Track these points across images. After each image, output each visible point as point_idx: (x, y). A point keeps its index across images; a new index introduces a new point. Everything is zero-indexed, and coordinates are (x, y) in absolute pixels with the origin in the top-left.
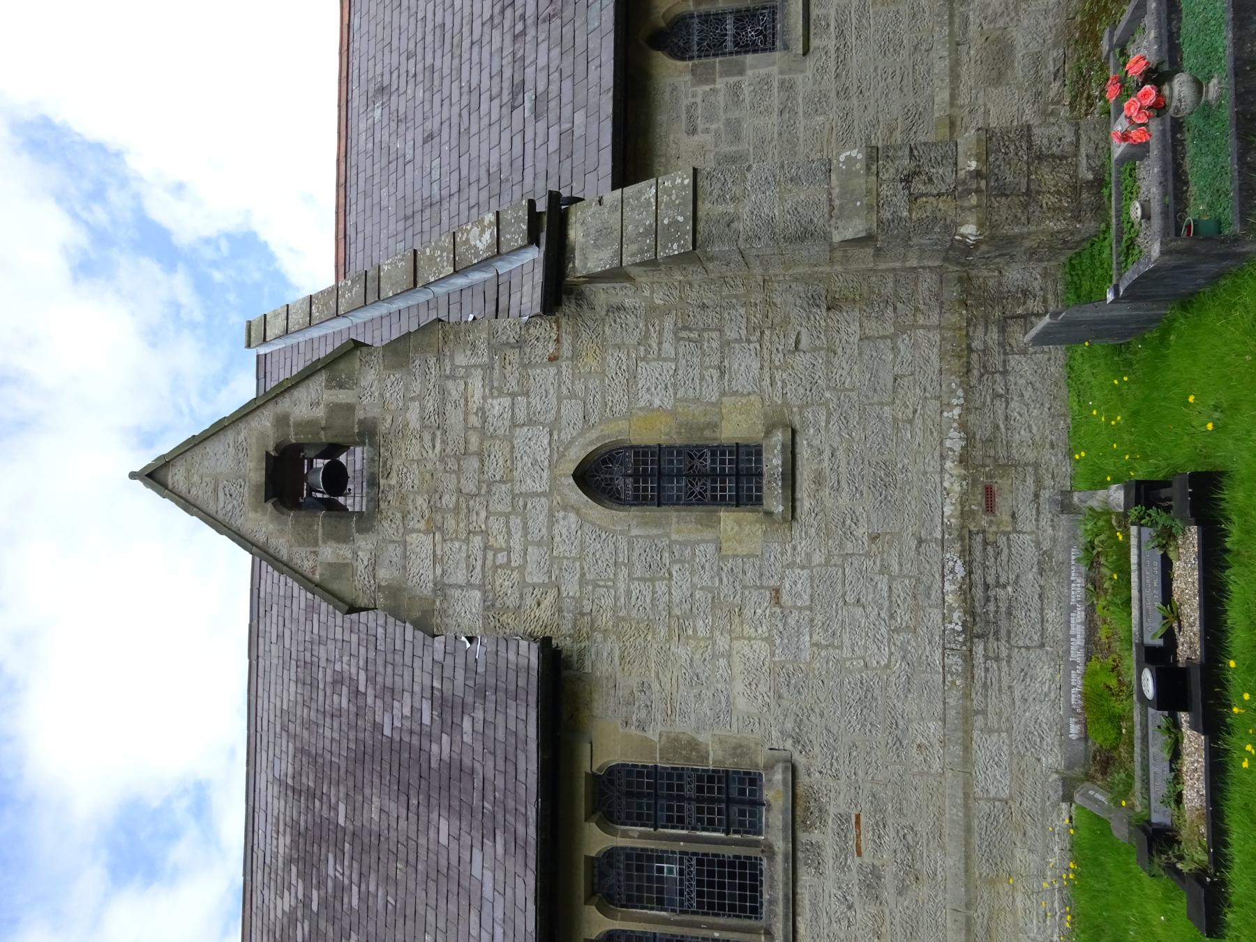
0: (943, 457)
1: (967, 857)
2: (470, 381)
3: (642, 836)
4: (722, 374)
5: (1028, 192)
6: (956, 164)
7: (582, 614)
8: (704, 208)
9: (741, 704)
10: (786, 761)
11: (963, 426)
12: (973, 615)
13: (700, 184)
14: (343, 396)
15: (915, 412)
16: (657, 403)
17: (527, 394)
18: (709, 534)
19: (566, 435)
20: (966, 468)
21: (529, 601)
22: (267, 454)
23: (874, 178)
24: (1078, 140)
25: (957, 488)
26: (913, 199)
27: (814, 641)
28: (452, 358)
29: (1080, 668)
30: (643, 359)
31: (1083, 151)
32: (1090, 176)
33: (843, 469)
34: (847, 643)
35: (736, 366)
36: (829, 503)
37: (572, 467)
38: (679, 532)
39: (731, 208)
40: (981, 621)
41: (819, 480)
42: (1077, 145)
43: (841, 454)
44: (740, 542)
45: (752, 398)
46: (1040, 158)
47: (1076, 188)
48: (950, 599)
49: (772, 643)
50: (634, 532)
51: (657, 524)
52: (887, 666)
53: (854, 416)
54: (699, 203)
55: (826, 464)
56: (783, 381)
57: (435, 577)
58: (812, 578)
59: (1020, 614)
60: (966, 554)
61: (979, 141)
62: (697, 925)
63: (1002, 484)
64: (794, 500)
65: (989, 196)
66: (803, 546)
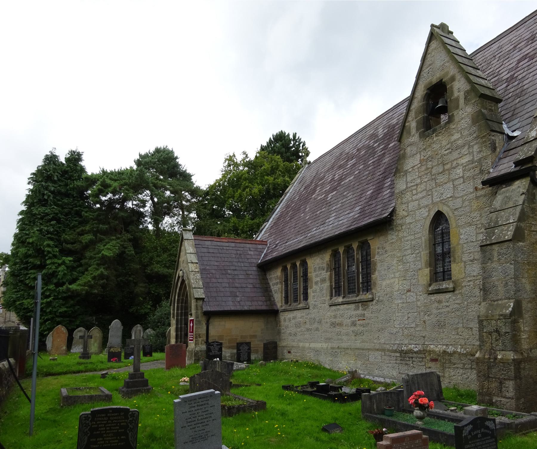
0: (447, 345)
1: (358, 349)
2: (468, 155)
3: (358, 259)
4: (471, 261)
5: (489, 377)
6: (503, 350)
7: (401, 227)
8: (496, 247)
9: (384, 283)
10: (373, 298)
11: (455, 352)
12: (405, 353)
13: (506, 243)
14: (462, 101)
15: (461, 335)
16: (462, 237)
17: (464, 182)
18: (423, 265)
19: (451, 204)
20: (442, 353)
21: (404, 206)
22: (442, 80)
23: (498, 318)
24: (507, 398)
25: (437, 349)
26: (490, 333)
27: (400, 304)
28: (476, 143)
29: (372, 379)
30: (476, 227)
31: (503, 399)
32: (494, 401)
33: (444, 310)
34: (400, 314)
35: (474, 266)
36: (433, 306)
37: (441, 210)
38: (424, 254)
39: (496, 259)
40: (405, 355)
41: (440, 302)
42: (505, 397)
43: (448, 309)
44: (422, 276)
45: (464, 274)
46: (501, 383)
47: (490, 395)
48: (410, 346)
49: (398, 291)
50: (423, 238)
51: (425, 246)
52: (395, 327)
53: (458, 313)
54: (498, 245)
55: (445, 304)
56: (469, 285)
57: (408, 170)
58: (414, 302)
59: (406, 367)
60: (419, 352)
61: (508, 360)
62: (344, 278)
63: (438, 364)
64: (433, 294)
65: (487, 362)
66: (422, 298)
